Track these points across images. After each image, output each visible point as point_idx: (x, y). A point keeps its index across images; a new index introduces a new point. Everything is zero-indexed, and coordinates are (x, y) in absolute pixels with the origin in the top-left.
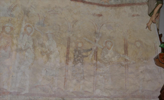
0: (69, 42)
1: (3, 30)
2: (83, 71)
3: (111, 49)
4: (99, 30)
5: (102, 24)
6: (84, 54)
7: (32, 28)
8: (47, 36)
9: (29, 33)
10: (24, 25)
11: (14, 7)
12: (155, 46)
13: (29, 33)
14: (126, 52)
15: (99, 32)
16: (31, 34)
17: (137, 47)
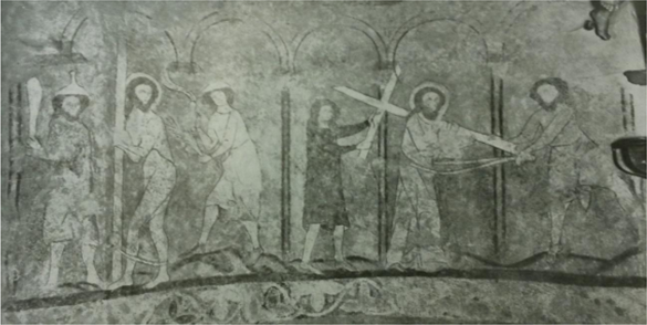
0: (286, 115)
1: (55, 110)
2: (342, 197)
3: (440, 117)
4: (391, 55)
5: (403, 30)
6: (341, 142)
7: (154, 86)
8: (211, 102)
9: (145, 103)
10: (122, 83)
11: (77, 30)
12: (623, 96)
13: (145, 103)
14: (497, 106)
15: (391, 60)
16: (153, 107)
17: (542, 103)
